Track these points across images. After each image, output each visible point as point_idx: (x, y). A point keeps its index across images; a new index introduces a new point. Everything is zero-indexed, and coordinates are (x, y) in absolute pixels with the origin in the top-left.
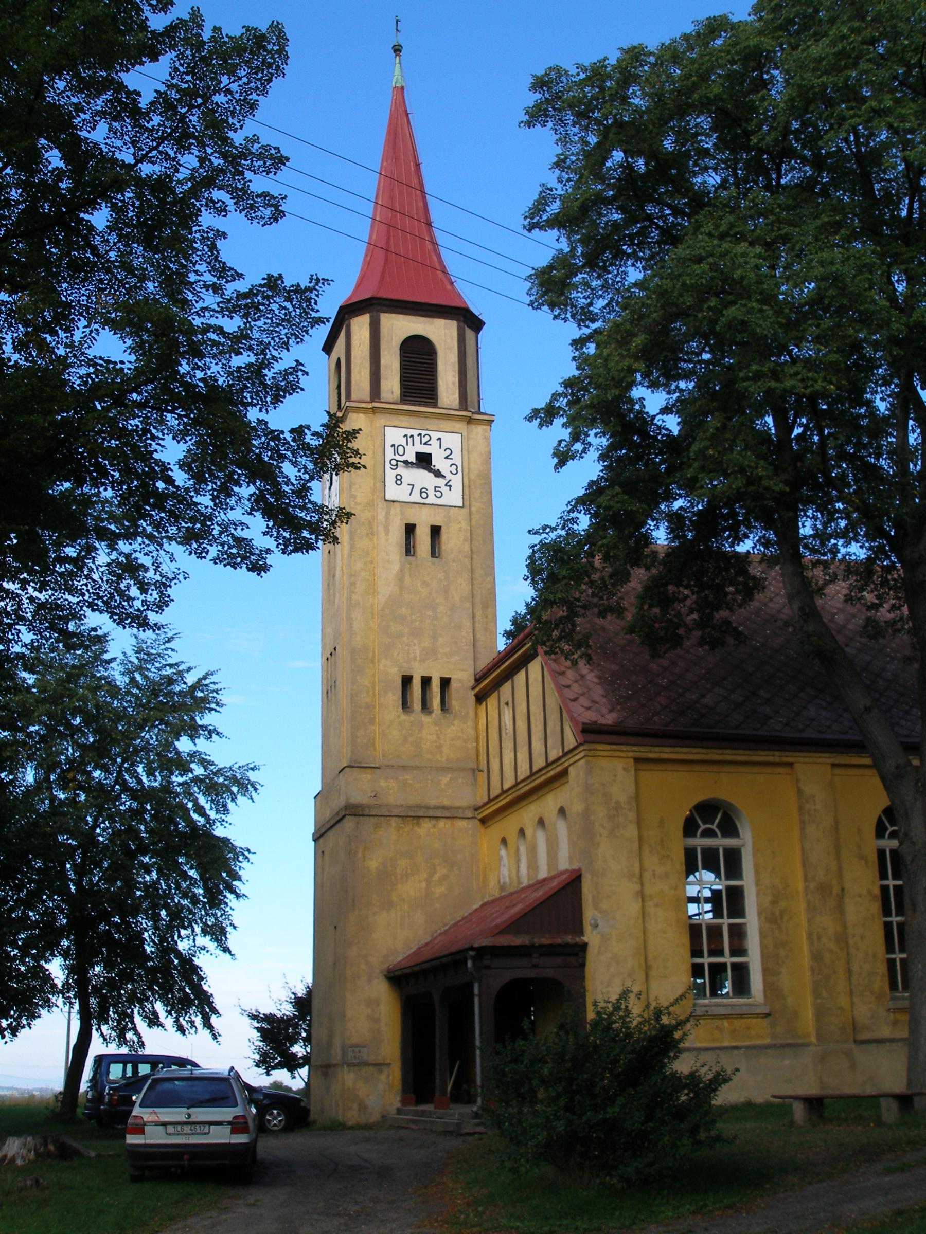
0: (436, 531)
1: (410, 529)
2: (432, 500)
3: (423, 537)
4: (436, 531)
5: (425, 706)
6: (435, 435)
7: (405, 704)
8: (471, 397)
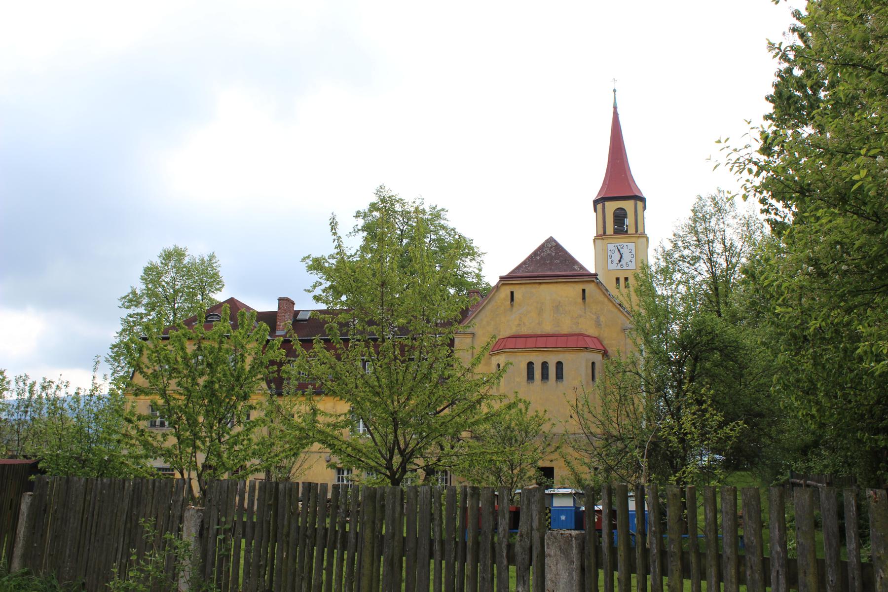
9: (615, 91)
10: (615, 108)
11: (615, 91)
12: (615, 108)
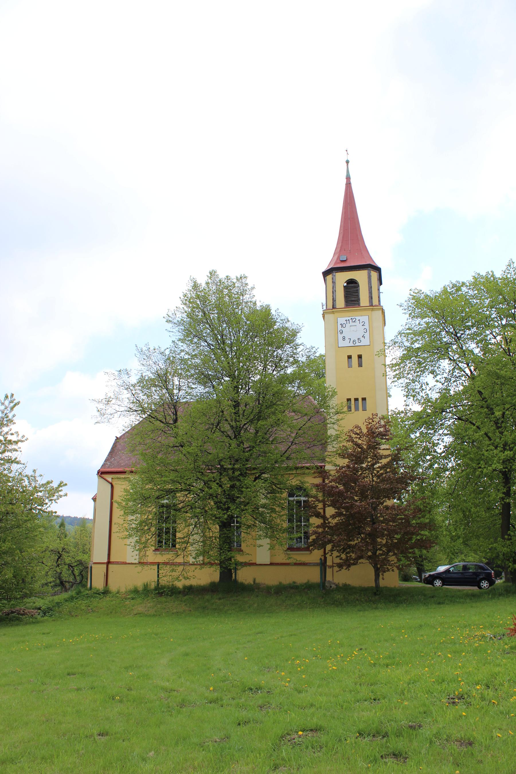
0: (360, 357)
1: (350, 357)
2: (358, 344)
3: (355, 359)
4: (360, 357)
5: (357, 409)
6: (358, 318)
7: (350, 366)
8: (375, 302)
9: (347, 162)
10: (348, 178)
11: (347, 162)
12: (348, 178)
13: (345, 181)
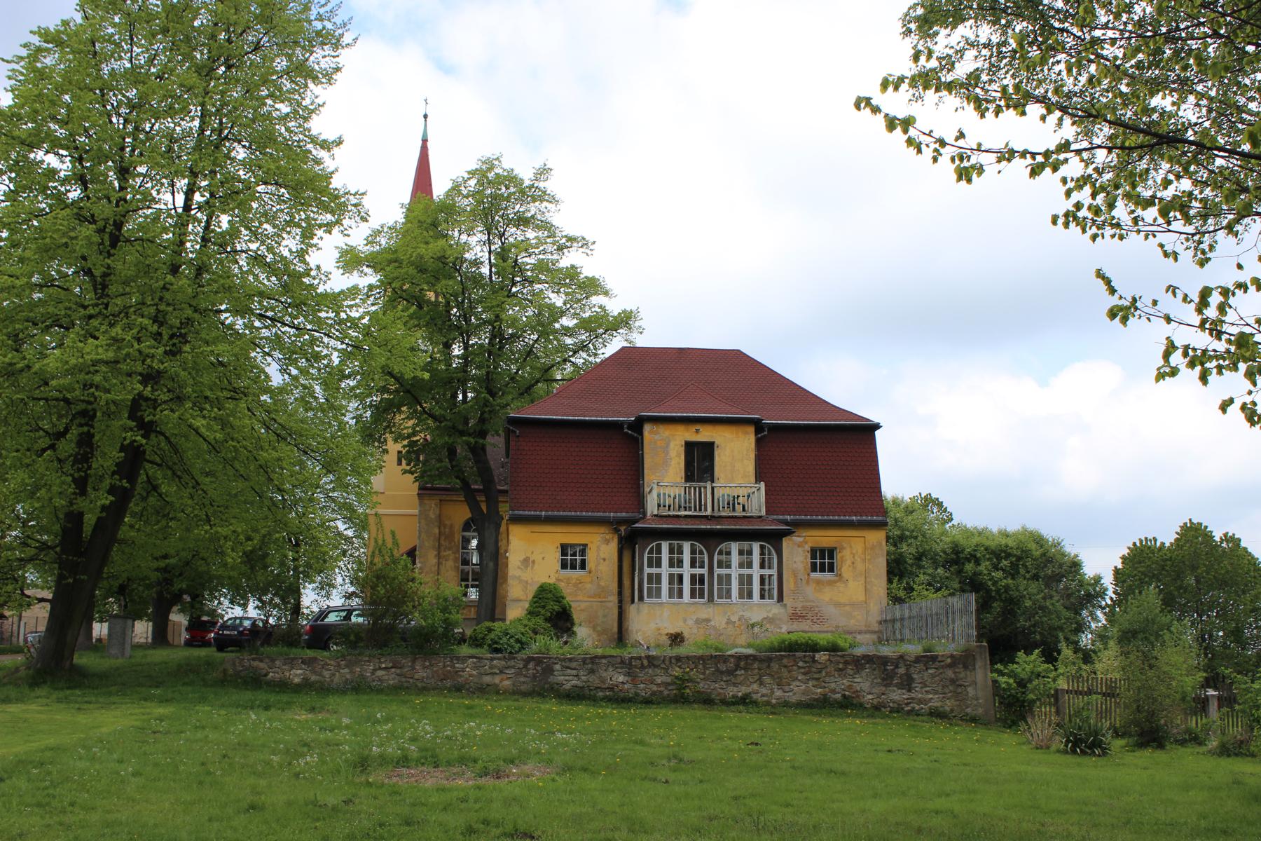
9: (426, 116)
10: (425, 141)
11: (426, 116)
12: (425, 141)
13: (420, 143)
